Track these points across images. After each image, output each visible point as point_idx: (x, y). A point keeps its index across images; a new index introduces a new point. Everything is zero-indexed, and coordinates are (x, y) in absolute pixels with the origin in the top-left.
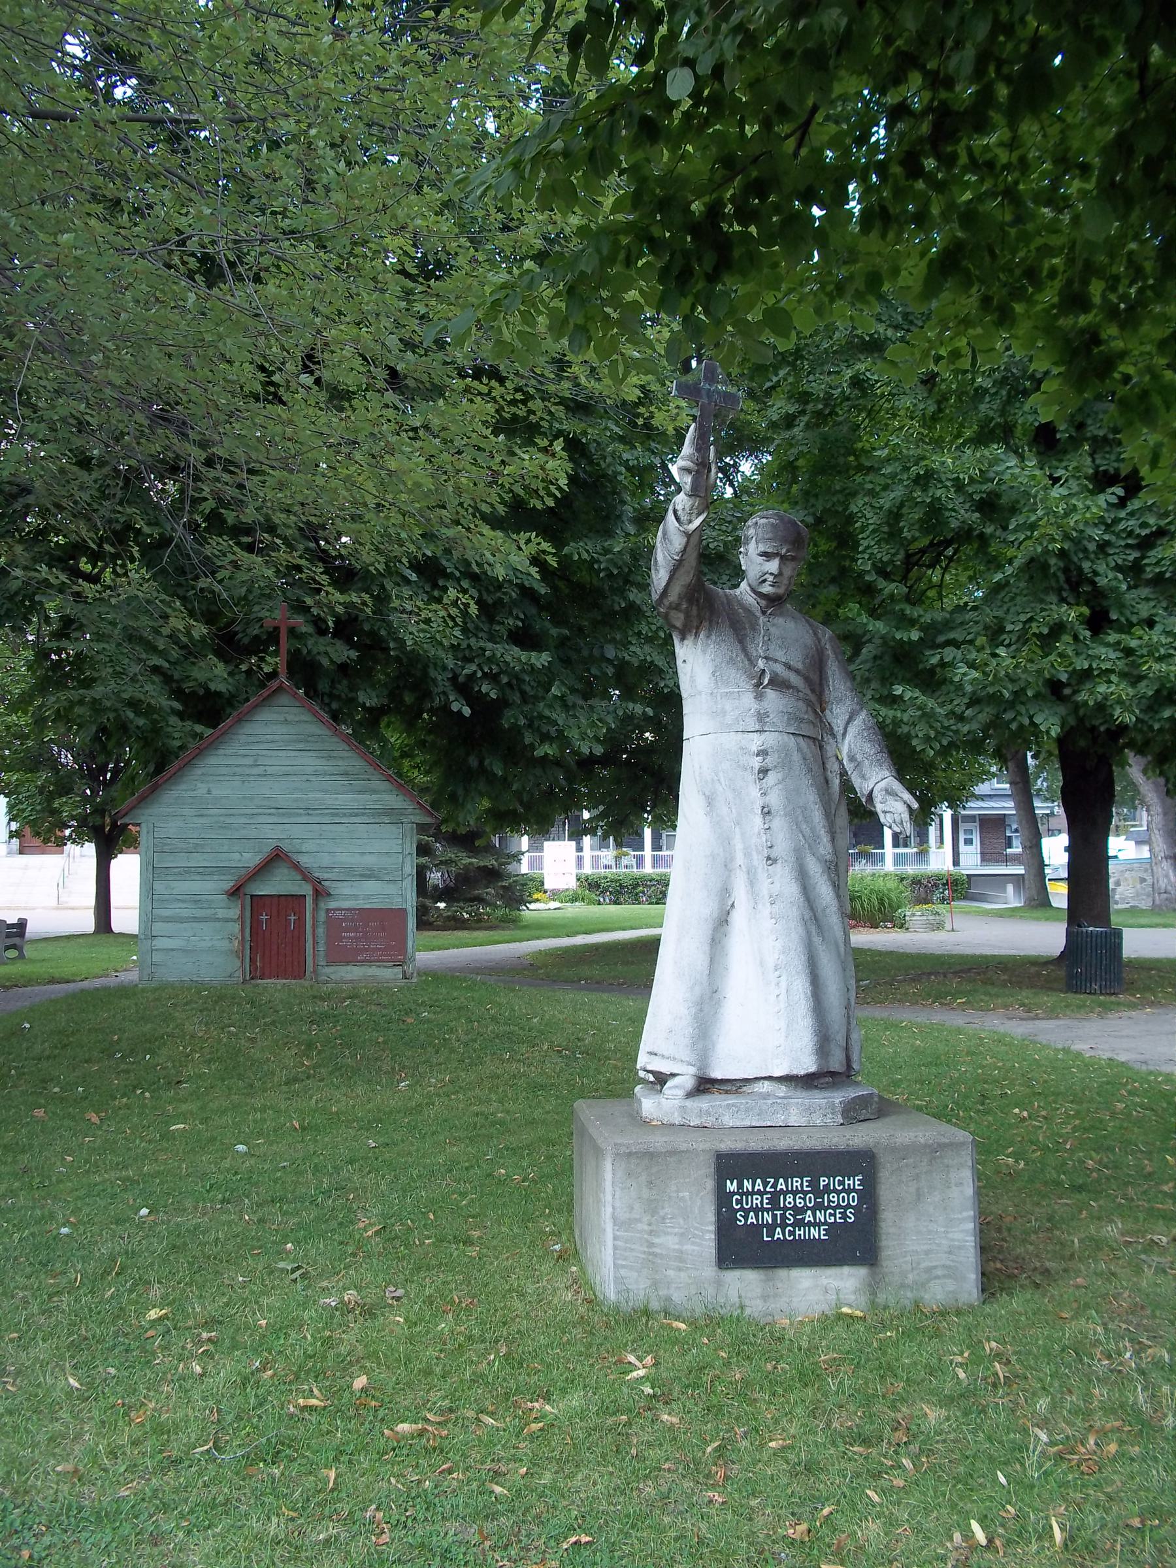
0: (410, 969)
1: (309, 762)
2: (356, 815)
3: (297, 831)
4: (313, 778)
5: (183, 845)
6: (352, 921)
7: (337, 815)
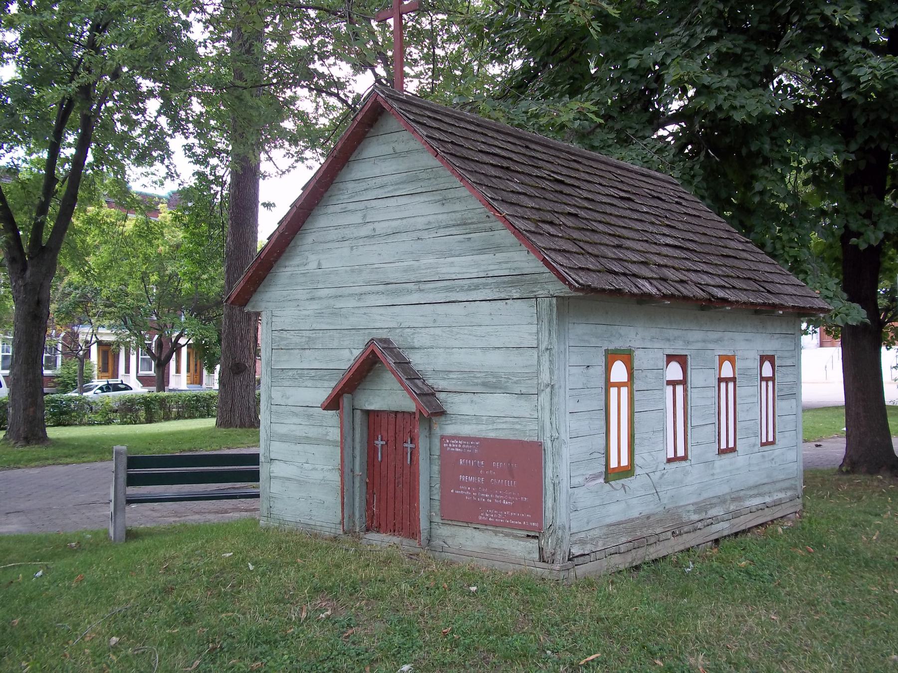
0: (549, 544)
1: (422, 210)
2: (477, 288)
3: (410, 317)
4: (425, 235)
5: (296, 340)
6: (472, 456)
7: (453, 291)
